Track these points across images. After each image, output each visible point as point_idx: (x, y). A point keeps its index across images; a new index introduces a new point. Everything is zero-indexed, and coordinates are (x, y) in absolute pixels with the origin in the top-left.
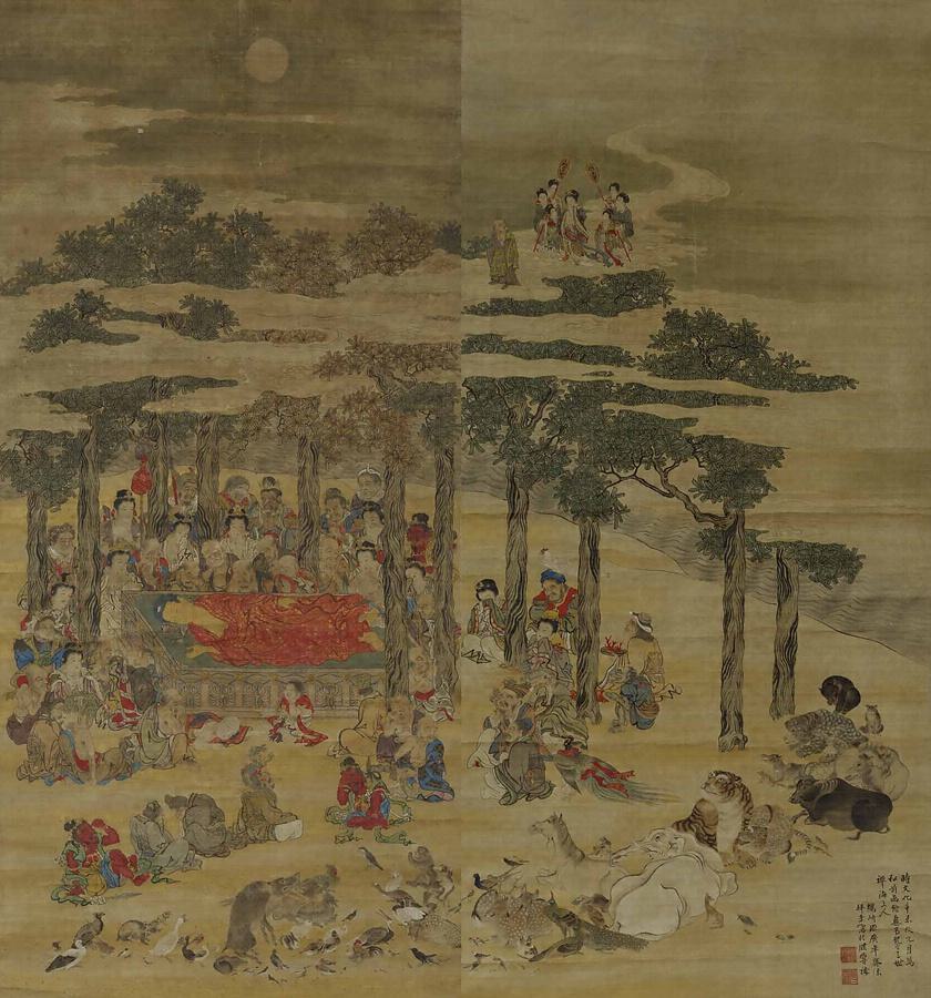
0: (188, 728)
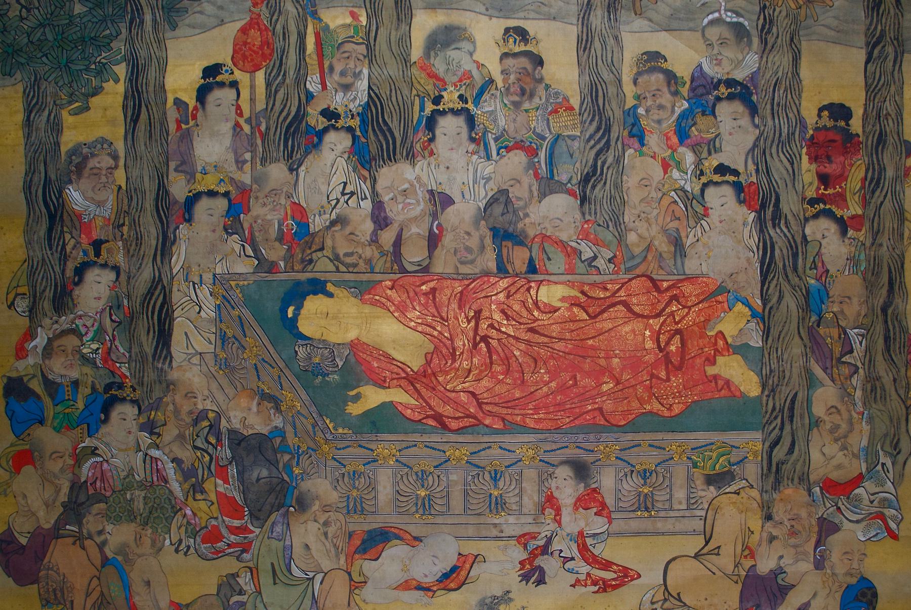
0: (350, 559)
